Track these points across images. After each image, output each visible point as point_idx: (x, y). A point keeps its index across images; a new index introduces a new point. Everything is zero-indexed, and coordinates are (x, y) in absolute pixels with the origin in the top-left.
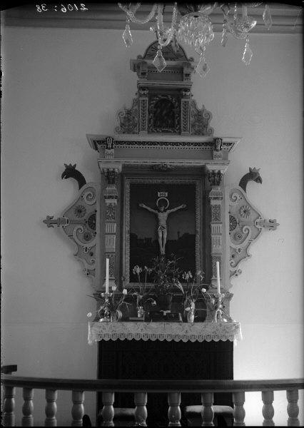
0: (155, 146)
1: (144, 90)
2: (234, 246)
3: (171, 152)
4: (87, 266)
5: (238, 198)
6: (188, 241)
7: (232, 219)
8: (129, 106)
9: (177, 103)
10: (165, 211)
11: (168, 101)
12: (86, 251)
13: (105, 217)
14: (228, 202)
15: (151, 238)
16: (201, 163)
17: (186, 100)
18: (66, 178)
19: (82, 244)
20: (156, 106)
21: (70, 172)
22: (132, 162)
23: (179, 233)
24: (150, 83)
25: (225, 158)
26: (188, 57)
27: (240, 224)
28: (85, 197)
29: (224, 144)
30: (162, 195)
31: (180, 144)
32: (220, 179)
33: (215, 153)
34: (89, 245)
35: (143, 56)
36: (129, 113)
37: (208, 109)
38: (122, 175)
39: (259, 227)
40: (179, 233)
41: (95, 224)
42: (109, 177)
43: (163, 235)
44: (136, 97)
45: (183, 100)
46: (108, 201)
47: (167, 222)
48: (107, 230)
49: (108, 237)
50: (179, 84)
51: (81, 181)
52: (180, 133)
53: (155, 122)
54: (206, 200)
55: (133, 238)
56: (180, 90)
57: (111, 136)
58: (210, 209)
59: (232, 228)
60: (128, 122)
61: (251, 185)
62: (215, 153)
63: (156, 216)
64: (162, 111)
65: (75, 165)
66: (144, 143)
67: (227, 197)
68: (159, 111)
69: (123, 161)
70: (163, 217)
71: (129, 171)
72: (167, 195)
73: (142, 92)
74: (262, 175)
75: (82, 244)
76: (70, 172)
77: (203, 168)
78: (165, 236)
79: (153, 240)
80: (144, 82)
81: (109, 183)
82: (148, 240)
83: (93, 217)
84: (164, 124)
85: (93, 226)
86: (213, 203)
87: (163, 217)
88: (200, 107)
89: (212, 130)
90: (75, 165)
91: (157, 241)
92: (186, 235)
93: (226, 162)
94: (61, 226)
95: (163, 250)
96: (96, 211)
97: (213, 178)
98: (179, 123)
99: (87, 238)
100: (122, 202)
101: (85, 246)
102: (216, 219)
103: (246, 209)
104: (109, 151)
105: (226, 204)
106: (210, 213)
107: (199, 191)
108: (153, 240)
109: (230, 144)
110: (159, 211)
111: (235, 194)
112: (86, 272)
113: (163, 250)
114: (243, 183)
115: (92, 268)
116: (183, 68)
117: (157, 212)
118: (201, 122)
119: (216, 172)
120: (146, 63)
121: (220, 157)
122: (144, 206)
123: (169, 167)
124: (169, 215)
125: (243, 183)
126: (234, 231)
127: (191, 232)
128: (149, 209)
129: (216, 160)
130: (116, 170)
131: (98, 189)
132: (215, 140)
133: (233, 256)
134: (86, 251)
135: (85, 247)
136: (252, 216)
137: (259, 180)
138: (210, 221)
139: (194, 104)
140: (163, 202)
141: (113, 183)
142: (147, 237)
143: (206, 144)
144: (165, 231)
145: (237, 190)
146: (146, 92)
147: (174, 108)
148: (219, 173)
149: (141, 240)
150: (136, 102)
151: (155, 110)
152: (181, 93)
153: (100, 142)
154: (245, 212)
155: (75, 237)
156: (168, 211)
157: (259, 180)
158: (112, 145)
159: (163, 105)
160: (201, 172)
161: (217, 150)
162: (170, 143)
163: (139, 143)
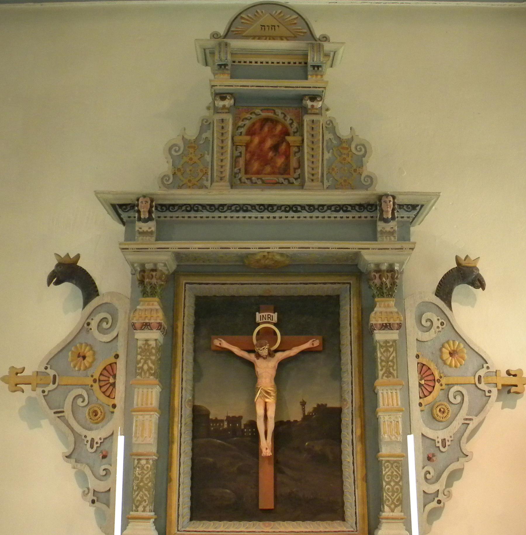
0: (247, 214)
1: (223, 98)
2: (430, 433)
3: (272, 233)
4: (94, 484)
5: (437, 323)
6: (327, 422)
7: (424, 370)
8: (192, 133)
9: (295, 125)
10: (271, 354)
11: (274, 122)
12: (92, 447)
13: (134, 371)
14: (413, 332)
15: (240, 418)
16: (353, 246)
17: (315, 118)
18: (57, 283)
19: (84, 432)
20: (251, 132)
21: (68, 272)
22: (195, 246)
23: (303, 404)
24: (238, 84)
25: (405, 237)
26: (318, 34)
27: (443, 381)
28: (94, 324)
29: (401, 206)
30: (266, 319)
31: (303, 207)
32: (393, 284)
33: (381, 225)
34: (98, 435)
35: (222, 32)
36: (191, 145)
37: (362, 135)
38: (173, 277)
39: (486, 388)
40: (303, 404)
41: (113, 385)
42: (146, 281)
43: (265, 411)
44: (206, 113)
45: (307, 119)
46: (141, 335)
47: (278, 379)
48: (137, 401)
49: (138, 418)
50: (297, 85)
51: (88, 288)
52: (302, 186)
53: (247, 164)
54: (365, 332)
55: (199, 416)
56: (300, 98)
57: (146, 191)
58: (374, 350)
59: (426, 390)
60: (188, 161)
61: (460, 291)
62: (381, 225)
63: (251, 365)
64: (262, 142)
65: (78, 257)
66: (221, 208)
67: (411, 322)
68: (256, 140)
69: (175, 245)
70: (266, 370)
71: (188, 266)
72: (275, 320)
73: (220, 103)
74: (484, 270)
75: (84, 432)
76: (68, 272)
77: (357, 255)
78: (271, 413)
79: (244, 422)
80: (225, 82)
81: (145, 294)
82: (234, 420)
83: (110, 370)
84: (268, 169)
85: (108, 388)
86: (379, 336)
87: (266, 370)
88: (344, 132)
89: (371, 179)
90: (78, 257)
91: (253, 425)
92: (321, 409)
93: (406, 245)
94: (39, 390)
95: (266, 446)
96: (117, 356)
97: (377, 281)
98: (300, 164)
99: (97, 416)
100: (174, 334)
101: (90, 435)
102: (389, 374)
103: (456, 347)
104: (145, 227)
105: (406, 329)
106: (374, 360)
107: (349, 312)
108: (244, 422)
109: (414, 207)
110: (258, 356)
111: (358, 147)
112: (91, 496)
113: (266, 446)
114: (445, 290)
115: (101, 486)
116: (306, 55)
117: (251, 357)
118: (349, 159)
119: (384, 267)
120: (226, 44)
121: (392, 233)
122: (225, 345)
123: (278, 257)
124: (282, 364)
125: (445, 290)
126: (430, 398)
127: (332, 403)
128: (236, 350)
129: (383, 242)
130: (160, 267)
131: (123, 308)
132: (380, 198)
133: (429, 459)
134: (92, 447)
135: (89, 439)
136: (472, 363)
137: (479, 283)
138: (376, 378)
139: (331, 126)
140: (268, 334)
141: (153, 295)
142: (231, 415)
143: (361, 207)
144: (271, 401)
145: (427, 305)
146: (228, 102)
147: (288, 135)
148: (391, 269)
149: (216, 421)
150: (206, 125)
151: (248, 138)
152: (301, 104)
153: (121, 206)
154: (451, 354)
155: (68, 414)
156: (280, 356)
157: (479, 283)
158: (150, 212)
159: (266, 129)
160: (351, 268)
161: (386, 221)
162: (279, 207)
163: (212, 207)
